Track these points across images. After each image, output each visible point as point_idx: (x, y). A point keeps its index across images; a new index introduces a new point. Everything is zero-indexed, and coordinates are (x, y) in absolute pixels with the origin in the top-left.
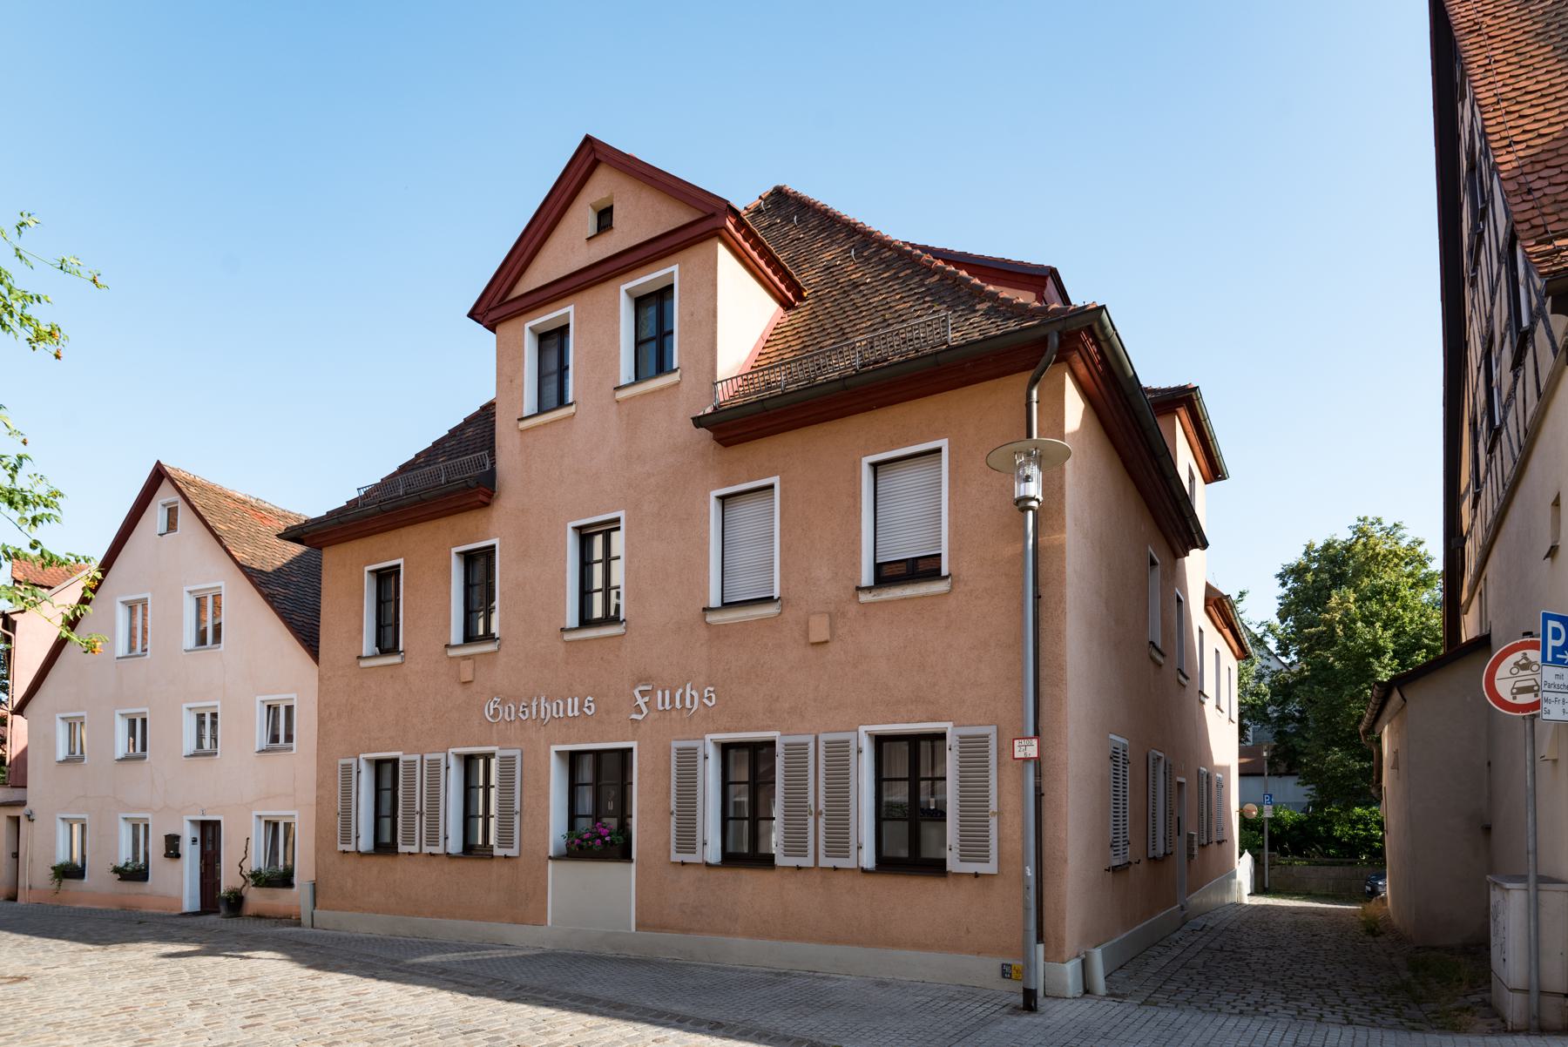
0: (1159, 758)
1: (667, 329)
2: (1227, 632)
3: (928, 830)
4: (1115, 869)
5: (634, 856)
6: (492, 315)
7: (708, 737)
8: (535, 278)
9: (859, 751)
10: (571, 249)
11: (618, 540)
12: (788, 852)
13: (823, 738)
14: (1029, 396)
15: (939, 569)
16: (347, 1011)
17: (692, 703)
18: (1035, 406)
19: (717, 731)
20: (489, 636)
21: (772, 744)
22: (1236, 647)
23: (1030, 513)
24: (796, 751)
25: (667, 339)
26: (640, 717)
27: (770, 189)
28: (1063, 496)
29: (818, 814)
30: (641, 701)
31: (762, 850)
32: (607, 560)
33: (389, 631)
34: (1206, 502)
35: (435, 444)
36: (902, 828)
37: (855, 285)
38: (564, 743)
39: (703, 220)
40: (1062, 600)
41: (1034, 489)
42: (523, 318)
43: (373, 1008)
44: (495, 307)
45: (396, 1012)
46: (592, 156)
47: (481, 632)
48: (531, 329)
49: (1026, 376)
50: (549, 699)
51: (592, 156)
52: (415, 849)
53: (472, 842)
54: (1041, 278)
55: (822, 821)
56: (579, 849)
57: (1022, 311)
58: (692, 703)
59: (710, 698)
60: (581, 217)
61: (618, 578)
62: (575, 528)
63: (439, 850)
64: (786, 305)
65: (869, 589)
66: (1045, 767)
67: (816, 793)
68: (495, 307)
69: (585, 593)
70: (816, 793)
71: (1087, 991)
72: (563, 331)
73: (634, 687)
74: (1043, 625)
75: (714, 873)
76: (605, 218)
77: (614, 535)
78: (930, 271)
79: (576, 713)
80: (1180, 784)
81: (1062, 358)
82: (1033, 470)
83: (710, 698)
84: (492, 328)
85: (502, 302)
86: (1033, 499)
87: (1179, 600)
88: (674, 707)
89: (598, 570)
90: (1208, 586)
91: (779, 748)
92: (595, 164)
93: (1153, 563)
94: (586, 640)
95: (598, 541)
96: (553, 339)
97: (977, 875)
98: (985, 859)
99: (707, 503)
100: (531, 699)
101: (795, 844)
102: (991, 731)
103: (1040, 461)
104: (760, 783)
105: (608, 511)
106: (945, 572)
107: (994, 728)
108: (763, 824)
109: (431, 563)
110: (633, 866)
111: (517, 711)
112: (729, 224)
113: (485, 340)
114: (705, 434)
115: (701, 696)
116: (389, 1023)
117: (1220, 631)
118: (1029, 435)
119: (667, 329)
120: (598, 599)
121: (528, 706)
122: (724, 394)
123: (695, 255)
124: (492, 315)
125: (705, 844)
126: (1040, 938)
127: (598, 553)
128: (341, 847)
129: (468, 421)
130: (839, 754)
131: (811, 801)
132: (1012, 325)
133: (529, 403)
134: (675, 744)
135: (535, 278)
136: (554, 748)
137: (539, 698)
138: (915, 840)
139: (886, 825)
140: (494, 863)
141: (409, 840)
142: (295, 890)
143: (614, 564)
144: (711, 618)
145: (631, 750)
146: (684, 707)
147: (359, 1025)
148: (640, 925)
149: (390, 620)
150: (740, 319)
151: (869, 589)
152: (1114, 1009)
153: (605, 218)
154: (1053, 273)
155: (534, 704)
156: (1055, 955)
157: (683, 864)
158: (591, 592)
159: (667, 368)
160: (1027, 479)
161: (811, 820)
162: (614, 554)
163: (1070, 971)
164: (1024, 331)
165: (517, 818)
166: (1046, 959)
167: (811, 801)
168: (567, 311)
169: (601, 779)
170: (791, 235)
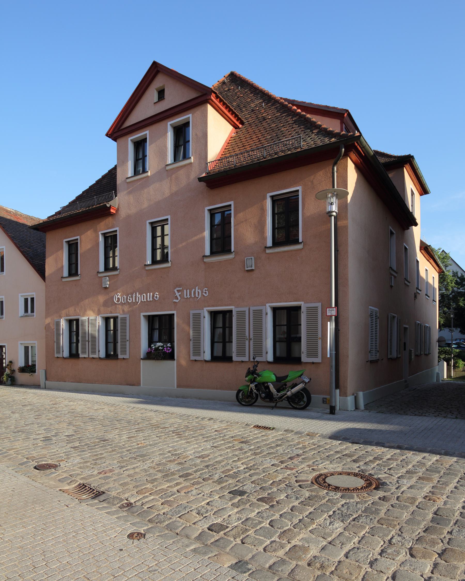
0: (394, 317)
1: (187, 140)
2: (432, 261)
3: (295, 346)
4: (372, 362)
5: (175, 358)
6: (115, 135)
7: (205, 309)
8: (134, 119)
9: (267, 314)
10: (148, 107)
11: (167, 229)
12: (238, 355)
13: (252, 308)
14: (333, 169)
15: (298, 239)
16: (70, 414)
17: (198, 295)
18: (335, 173)
19: (209, 306)
20: (114, 268)
21: (231, 312)
22: (437, 268)
23: (333, 217)
24: (241, 314)
25: (187, 144)
26: (177, 301)
27: (229, 73)
28: (347, 209)
29: (250, 339)
30: (177, 294)
31: (228, 355)
32: (163, 236)
33: (74, 266)
34: (417, 205)
35: (90, 187)
36: (284, 345)
37: (264, 119)
38: (146, 312)
39: (201, 96)
40: (347, 252)
41: (334, 208)
42: (128, 136)
43: (81, 413)
44: (117, 132)
45: (89, 414)
46: (156, 69)
47: (111, 266)
48: (131, 140)
49: (332, 161)
50: (140, 294)
51: (156, 69)
52: (86, 356)
53: (109, 353)
54: (343, 116)
55: (252, 342)
56: (152, 355)
57: (330, 134)
58: (198, 295)
59: (206, 293)
60: (152, 94)
61: (167, 241)
62: (150, 223)
63: (96, 356)
64: (236, 127)
65: (270, 248)
66: (340, 319)
67: (249, 331)
68: (117, 132)
69: (154, 250)
70: (249, 331)
71: (357, 408)
72: (145, 140)
73: (175, 289)
74: (340, 262)
75: (208, 364)
76: (161, 94)
77: (165, 226)
78: (294, 114)
79: (151, 299)
80: (405, 329)
81: (346, 155)
82: (334, 200)
83: (206, 293)
84: (115, 140)
85: (119, 130)
86: (334, 212)
87: (406, 248)
88: (191, 297)
89: (159, 240)
90: (421, 240)
91: (234, 313)
92: (157, 72)
93: (392, 233)
94: (155, 269)
95: (159, 229)
96: (140, 145)
97: (313, 363)
98: (316, 356)
99: (204, 212)
100: (133, 294)
101: (241, 352)
102: (319, 305)
103: (337, 196)
104: (227, 326)
105: (163, 216)
106: (300, 240)
107: (320, 304)
108: (228, 344)
109: (90, 239)
110: (175, 362)
111: (127, 299)
112: (212, 97)
113: (112, 145)
114: (203, 184)
115: (202, 292)
116: (88, 418)
117: (428, 261)
118: (333, 187)
119: (187, 140)
120: (159, 251)
121: (132, 297)
122: (210, 167)
123: (198, 112)
124: (115, 135)
125: (204, 352)
126: (337, 387)
127: (159, 233)
128: (56, 355)
129: (104, 177)
130: (258, 315)
131: (247, 334)
132: (327, 141)
133: (130, 172)
134: (192, 312)
135: (134, 119)
136: (142, 314)
137: (136, 294)
138: (289, 350)
139: (278, 344)
140: (119, 361)
141: (84, 352)
142: (36, 373)
143: (165, 237)
144: (206, 260)
145: (173, 314)
146: (195, 296)
147: (77, 418)
148: (178, 386)
149: (74, 261)
150: (217, 133)
151: (270, 248)
152: (367, 413)
153: (161, 94)
154: (347, 111)
155: (134, 295)
156: (344, 394)
157: (196, 361)
158: (156, 249)
159: (187, 157)
160: (332, 204)
161: (247, 342)
162: (165, 233)
163: (350, 399)
164: (335, 138)
165: (128, 343)
166: (340, 395)
167: (247, 334)
168: (146, 133)
169: (161, 326)
170: (238, 95)
